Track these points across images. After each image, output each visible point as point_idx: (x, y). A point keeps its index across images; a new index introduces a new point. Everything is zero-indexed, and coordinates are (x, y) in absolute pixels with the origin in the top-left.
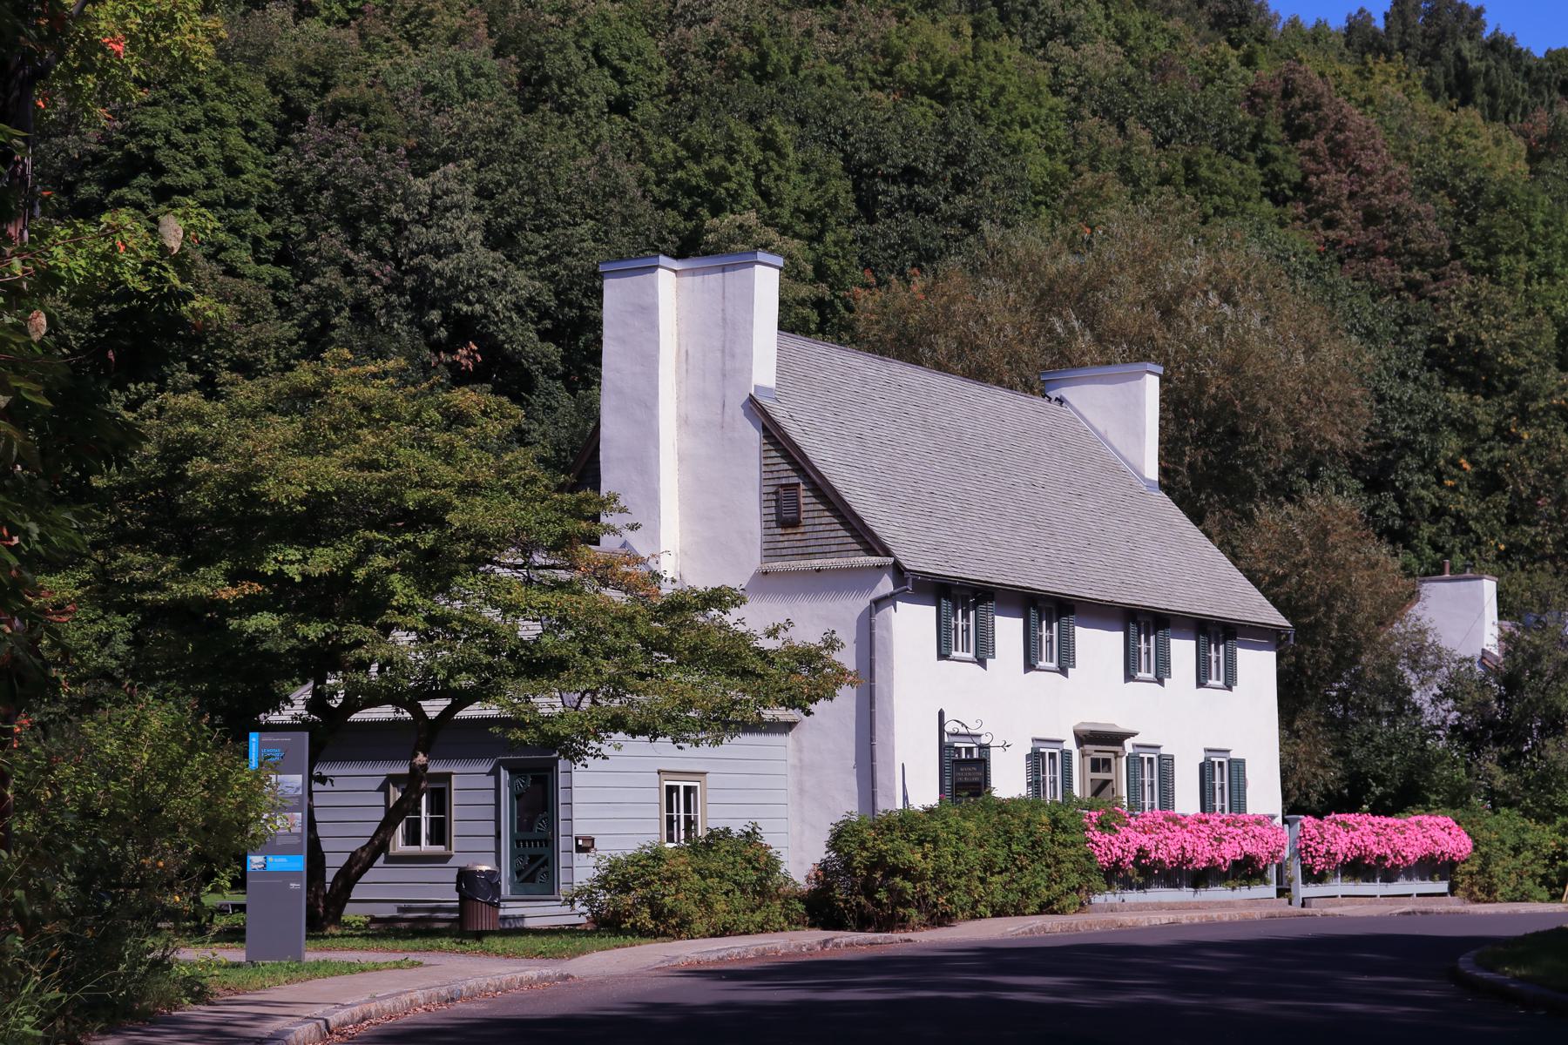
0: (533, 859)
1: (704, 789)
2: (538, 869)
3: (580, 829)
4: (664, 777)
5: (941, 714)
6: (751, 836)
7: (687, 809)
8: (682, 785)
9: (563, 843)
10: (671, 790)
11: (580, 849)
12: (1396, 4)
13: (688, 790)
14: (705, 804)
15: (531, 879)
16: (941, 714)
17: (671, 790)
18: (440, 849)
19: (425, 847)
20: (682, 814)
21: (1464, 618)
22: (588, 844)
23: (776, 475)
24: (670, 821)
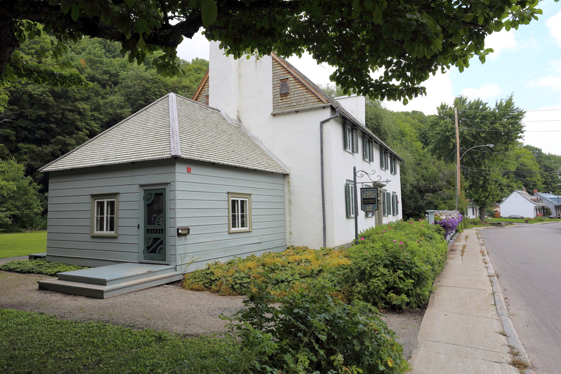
0: (156, 240)
1: (251, 202)
2: (152, 245)
3: (180, 223)
4: (230, 196)
5: (355, 168)
6: (521, 114)
7: (242, 211)
8: (240, 199)
9: (171, 232)
10: (234, 202)
11: (179, 235)
12: (548, 164)
13: (242, 202)
14: (251, 209)
15: (154, 251)
16: (355, 168)
17: (234, 202)
18: (112, 233)
19: (105, 232)
20: (240, 214)
21: (362, 88)
22: (185, 232)
23: (278, 76)
24: (234, 216)
